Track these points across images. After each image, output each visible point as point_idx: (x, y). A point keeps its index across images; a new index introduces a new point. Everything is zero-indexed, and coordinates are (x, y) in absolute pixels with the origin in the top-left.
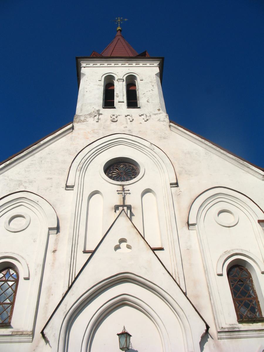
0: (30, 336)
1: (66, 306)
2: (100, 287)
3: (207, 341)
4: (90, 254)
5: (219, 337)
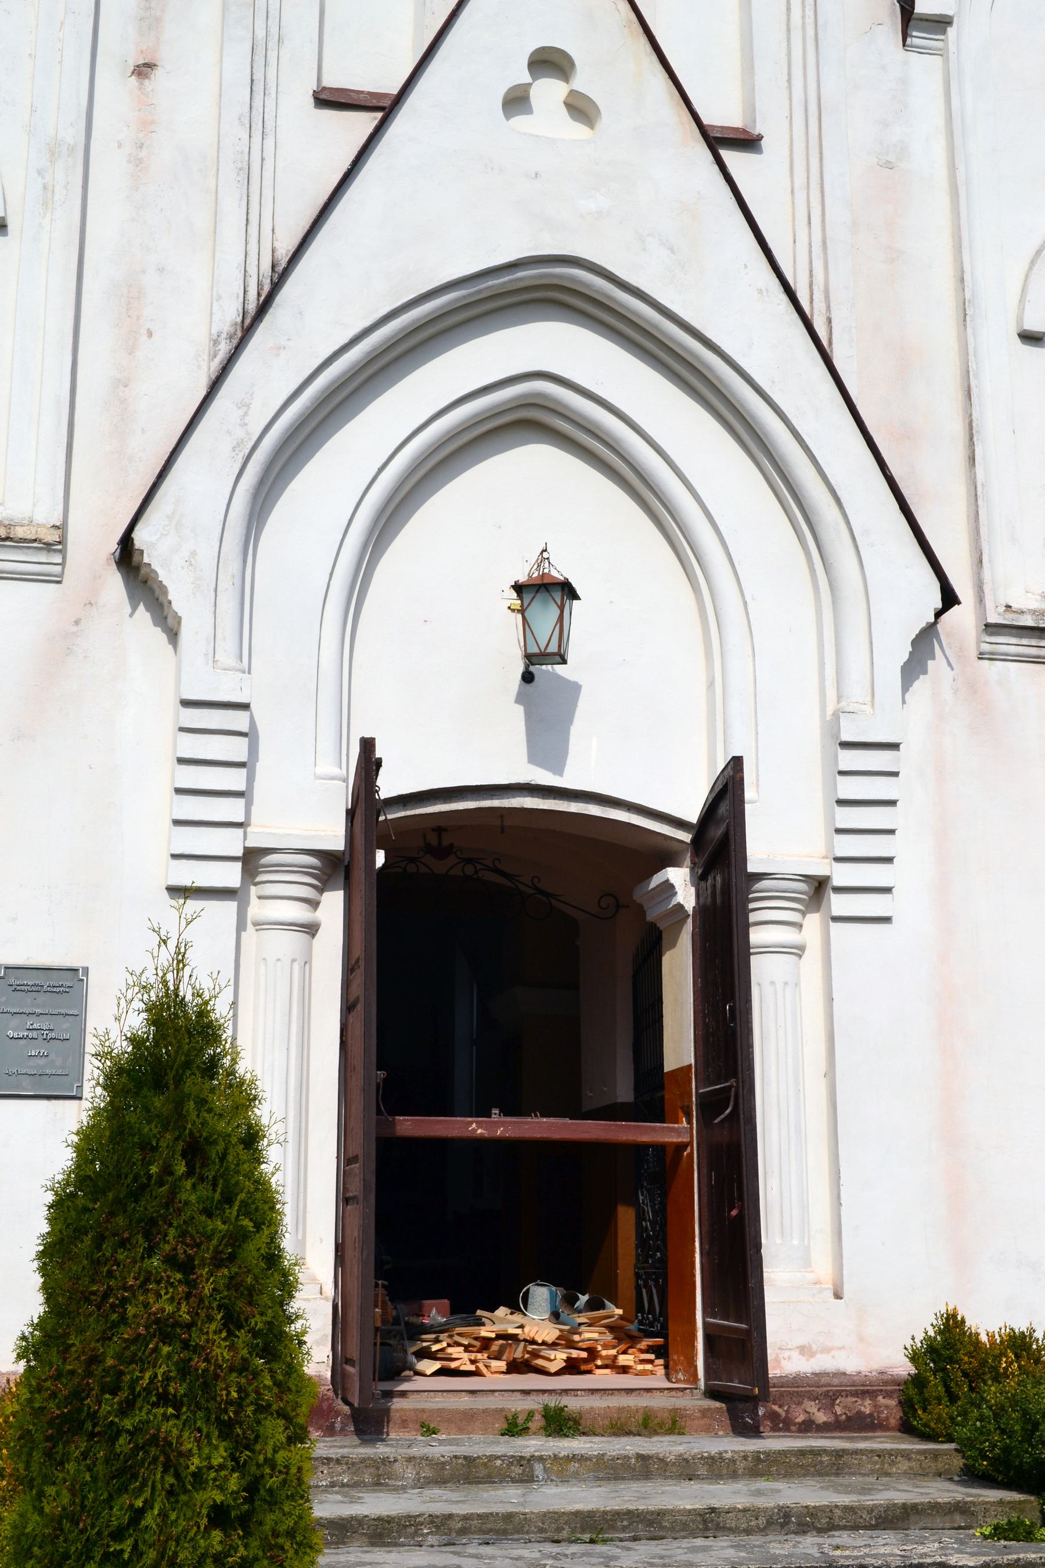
0: (49, 551)
1: (241, 412)
2: (418, 320)
3: (925, 672)
4: (367, 122)
5: (986, 647)
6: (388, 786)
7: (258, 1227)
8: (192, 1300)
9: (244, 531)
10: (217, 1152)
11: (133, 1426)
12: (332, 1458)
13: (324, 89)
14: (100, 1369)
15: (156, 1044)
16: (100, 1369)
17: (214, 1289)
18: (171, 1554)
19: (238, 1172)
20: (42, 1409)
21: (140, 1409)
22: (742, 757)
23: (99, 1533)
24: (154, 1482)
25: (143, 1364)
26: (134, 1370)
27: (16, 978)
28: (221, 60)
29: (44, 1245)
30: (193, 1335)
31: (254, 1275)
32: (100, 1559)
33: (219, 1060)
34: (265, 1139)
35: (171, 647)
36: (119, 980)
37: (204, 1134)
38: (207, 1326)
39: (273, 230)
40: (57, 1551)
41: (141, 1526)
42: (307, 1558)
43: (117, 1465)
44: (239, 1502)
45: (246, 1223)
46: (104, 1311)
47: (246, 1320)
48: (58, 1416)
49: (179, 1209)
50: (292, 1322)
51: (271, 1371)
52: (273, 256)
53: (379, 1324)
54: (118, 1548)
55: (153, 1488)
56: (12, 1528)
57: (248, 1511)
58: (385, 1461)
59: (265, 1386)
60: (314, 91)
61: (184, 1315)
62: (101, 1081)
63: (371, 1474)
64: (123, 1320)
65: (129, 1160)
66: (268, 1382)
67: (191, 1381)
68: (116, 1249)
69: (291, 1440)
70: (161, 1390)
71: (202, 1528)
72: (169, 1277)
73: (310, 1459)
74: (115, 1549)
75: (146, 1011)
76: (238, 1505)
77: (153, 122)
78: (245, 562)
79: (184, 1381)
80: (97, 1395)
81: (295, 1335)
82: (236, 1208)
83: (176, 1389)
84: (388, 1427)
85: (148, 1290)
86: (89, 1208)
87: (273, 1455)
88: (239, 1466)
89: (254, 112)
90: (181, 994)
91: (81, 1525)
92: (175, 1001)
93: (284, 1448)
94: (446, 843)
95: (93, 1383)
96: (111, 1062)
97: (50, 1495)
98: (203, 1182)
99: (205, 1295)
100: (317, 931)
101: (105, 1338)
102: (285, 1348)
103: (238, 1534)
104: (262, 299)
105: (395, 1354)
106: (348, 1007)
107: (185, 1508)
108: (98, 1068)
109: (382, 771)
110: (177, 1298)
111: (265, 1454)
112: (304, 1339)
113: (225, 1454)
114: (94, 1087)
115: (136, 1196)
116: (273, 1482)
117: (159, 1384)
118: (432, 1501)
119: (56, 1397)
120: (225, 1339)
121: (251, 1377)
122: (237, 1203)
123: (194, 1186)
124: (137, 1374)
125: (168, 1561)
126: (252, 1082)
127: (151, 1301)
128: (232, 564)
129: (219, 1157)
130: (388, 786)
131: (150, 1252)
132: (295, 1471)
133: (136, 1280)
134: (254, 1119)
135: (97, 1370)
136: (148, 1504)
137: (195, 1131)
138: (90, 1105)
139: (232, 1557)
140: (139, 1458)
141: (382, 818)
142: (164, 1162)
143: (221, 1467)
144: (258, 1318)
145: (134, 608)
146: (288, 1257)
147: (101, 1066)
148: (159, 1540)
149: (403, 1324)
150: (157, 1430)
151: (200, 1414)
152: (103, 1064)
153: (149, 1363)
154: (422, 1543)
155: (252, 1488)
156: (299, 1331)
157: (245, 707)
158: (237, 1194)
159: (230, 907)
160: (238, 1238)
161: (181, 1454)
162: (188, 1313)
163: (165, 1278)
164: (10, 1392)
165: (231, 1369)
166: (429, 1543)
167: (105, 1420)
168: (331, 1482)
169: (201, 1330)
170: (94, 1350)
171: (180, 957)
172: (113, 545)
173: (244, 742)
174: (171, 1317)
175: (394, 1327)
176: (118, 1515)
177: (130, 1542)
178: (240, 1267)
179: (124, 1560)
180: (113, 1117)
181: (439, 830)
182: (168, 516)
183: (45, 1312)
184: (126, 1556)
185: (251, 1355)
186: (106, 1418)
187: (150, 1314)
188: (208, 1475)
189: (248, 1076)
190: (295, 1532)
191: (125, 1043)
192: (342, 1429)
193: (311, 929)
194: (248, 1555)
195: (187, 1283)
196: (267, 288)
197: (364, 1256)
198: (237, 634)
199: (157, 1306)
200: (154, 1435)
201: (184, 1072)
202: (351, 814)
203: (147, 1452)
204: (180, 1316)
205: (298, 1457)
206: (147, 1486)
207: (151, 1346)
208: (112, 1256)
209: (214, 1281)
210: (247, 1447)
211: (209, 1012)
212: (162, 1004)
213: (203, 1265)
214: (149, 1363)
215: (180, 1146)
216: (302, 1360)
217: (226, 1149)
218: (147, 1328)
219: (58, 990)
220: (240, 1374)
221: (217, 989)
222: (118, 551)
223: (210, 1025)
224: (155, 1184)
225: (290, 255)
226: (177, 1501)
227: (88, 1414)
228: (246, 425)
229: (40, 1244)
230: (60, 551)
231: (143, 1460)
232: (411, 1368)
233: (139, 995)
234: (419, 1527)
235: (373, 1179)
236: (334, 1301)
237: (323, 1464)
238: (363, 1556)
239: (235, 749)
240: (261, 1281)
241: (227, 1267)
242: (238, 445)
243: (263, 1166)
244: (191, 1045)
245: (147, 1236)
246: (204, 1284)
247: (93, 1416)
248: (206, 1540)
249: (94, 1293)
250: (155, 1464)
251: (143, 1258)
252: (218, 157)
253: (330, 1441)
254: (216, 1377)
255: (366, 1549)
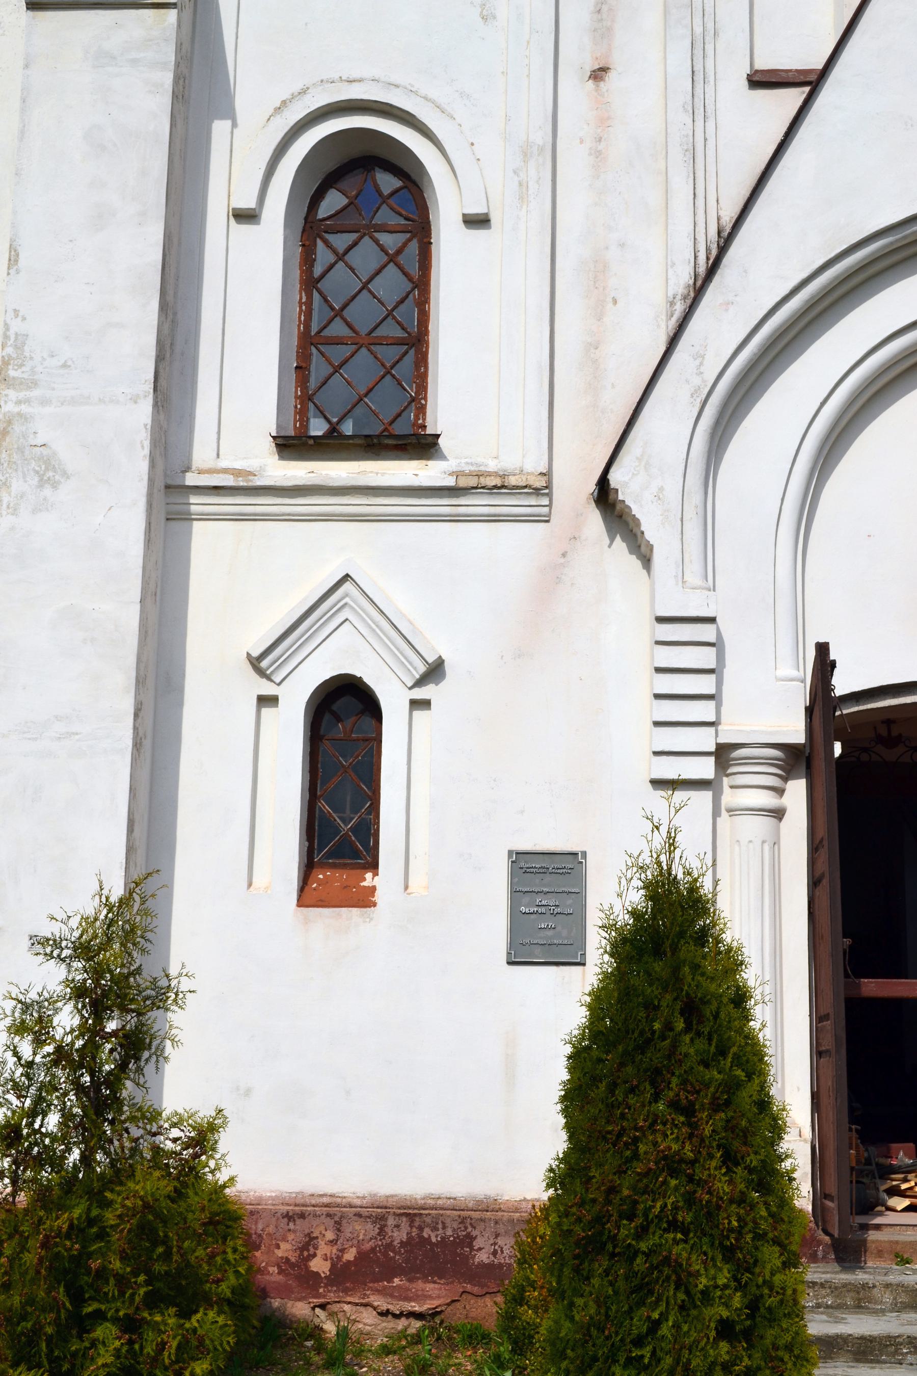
1: (697, 362)
6: (842, 684)
7: (749, 1076)
8: (694, 1139)
9: (705, 466)
10: (711, 1010)
11: (648, 1248)
12: (817, 1282)
13: (757, 71)
14: (618, 1198)
15: (654, 917)
16: (618, 1198)
17: (713, 1131)
18: (685, 1360)
19: (730, 1028)
20: (570, 1231)
21: (654, 1233)
22: (258, 696)
23: (622, 1340)
24: (668, 1298)
25: (655, 1194)
26: (647, 1200)
27: (526, 862)
28: (665, 58)
29: (565, 1090)
30: (696, 1171)
31: (747, 1118)
32: (624, 1362)
33: (709, 930)
34: (752, 999)
35: (645, 571)
36: (619, 863)
37: (699, 995)
38: (708, 1163)
39: (718, 201)
40: (587, 1354)
41: (657, 1336)
42: (804, 1370)
43: (636, 1282)
44: (742, 1317)
45: (739, 1073)
46: (619, 1148)
47: (743, 1158)
48: (584, 1238)
49: (679, 1060)
50: (782, 1161)
51: (765, 1203)
52: (718, 223)
53: (854, 1164)
54: (639, 1353)
55: (668, 1303)
56: (548, 1332)
57: (750, 1326)
58: (865, 1286)
59: (761, 1217)
60: (748, 75)
61: (689, 1153)
62: (608, 949)
63: (852, 1298)
64: (636, 1156)
65: (635, 1018)
66: (764, 1213)
67: (696, 1211)
68: (627, 1095)
69: (786, 1265)
70: (670, 1218)
71: (711, 1339)
72: (673, 1120)
73: (803, 1282)
74: (637, 1355)
75: (644, 888)
76: (742, 1320)
77: (609, 118)
78: (706, 493)
79: (690, 1211)
80: (616, 1221)
81: (785, 1173)
82: (730, 1060)
83: (684, 1217)
84: (865, 1256)
85: (656, 1130)
86: (602, 1060)
87: (771, 1278)
88: (741, 1287)
89: (696, 99)
90: (674, 873)
91: (607, 1332)
92: (668, 879)
93: (780, 1272)
94: (895, 733)
95: (612, 1210)
96: (616, 933)
97: (579, 1306)
98: (700, 1036)
99: (706, 1135)
100: (783, 815)
101: (621, 1172)
102: (777, 1184)
103: (743, 1346)
104: (711, 262)
105: (868, 1191)
106: (814, 883)
107: (695, 1322)
108: (605, 938)
109: (836, 671)
110: (681, 1138)
111: (764, 1276)
112: (794, 1176)
113: (728, 1275)
114: (602, 955)
115: (642, 1049)
116: (771, 1301)
117: (669, 1213)
118: (910, 1323)
119: (581, 1222)
120: (724, 1175)
121: (749, 1208)
122: (730, 1055)
123: (692, 1040)
124: (650, 1203)
125: (682, 1367)
126: (739, 949)
127: (659, 1140)
128: (695, 497)
129: (713, 1015)
130: (842, 684)
131: (656, 1098)
132: (791, 1292)
133: (646, 1121)
134: (741, 982)
135: (615, 1199)
136: (664, 1317)
137: (691, 992)
138: (600, 970)
139: (738, 1366)
140: (654, 1276)
141: (838, 713)
142: (666, 1020)
143: (726, 1287)
144: (752, 1156)
145: (612, 540)
146: (777, 1104)
147: (608, 937)
148: (674, 1348)
149: (874, 1165)
150: (668, 1252)
151: (705, 1240)
152: (609, 935)
153: (659, 1194)
154: (902, 1361)
155: (754, 1306)
156: (789, 1168)
157: (712, 620)
158: (730, 1048)
159: (704, 798)
160: (732, 1087)
161: (690, 1274)
162: (692, 1151)
163: (670, 1120)
164: (536, 1216)
165: (731, 1201)
166: (908, 1362)
167: (624, 1242)
168: (816, 1304)
169: (703, 1166)
170: (612, 1181)
171: (671, 841)
172: (591, 486)
173: (712, 651)
174: (677, 1155)
175: (866, 1167)
176: (638, 1326)
177: (649, 1348)
178: (735, 1112)
179: (644, 1364)
180: (620, 981)
181: (889, 722)
182: (637, 458)
183: (568, 1148)
184: (646, 1361)
185: (748, 1189)
186: (624, 1241)
187: (658, 1151)
188: (715, 1293)
189: (735, 944)
190: (793, 1346)
191: (627, 917)
192: (824, 1257)
193: (778, 814)
194: (752, 1364)
195: (689, 1124)
196: (714, 252)
197: (838, 1104)
198: (702, 556)
199: (665, 1144)
200: (667, 1256)
201: (679, 941)
202: (809, 711)
203: (661, 1272)
204: (685, 1154)
205: (792, 1279)
206: (662, 1300)
207: (661, 1179)
208: (624, 1101)
209: (712, 1123)
210: (748, 1270)
211: (698, 888)
212: (657, 882)
213: (703, 1109)
214: (659, 1194)
215: (679, 1005)
216: (793, 1194)
217: (718, 1008)
218: (656, 1163)
219: (561, 871)
220: (739, 1205)
221: (704, 868)
222: (596, 491)
223: (699, 900)
224: (658, 1038)
225: (733, 221)
226: (688, 1315)
227: (608, 1237)
228: (702, 373)
229: (562, 1090)
230: (547, 494)
231: (658, 1278)
232: (884, 1204)
233: (638, 875)
234: (899, 1347)
235: (843, 1035)
236: (812, 1143)
237: (809, 1287)
238: (849, 1370)
239: (705, 658)
240: (754, 1124)
241: (723, 1111)
242: (696, 391)
243: (752, 1023)
244: (684, 917)
245: (653, 1083)
246: (704, 1126)
247: (613, 1239)
248: (715, 1350)
249: (609, 1132)
250: (668, 1282)
251: (650, 1103)
252: (666, 142)
253: (814, 1267)
254: (719, 1207)
255: (850, 1364)
